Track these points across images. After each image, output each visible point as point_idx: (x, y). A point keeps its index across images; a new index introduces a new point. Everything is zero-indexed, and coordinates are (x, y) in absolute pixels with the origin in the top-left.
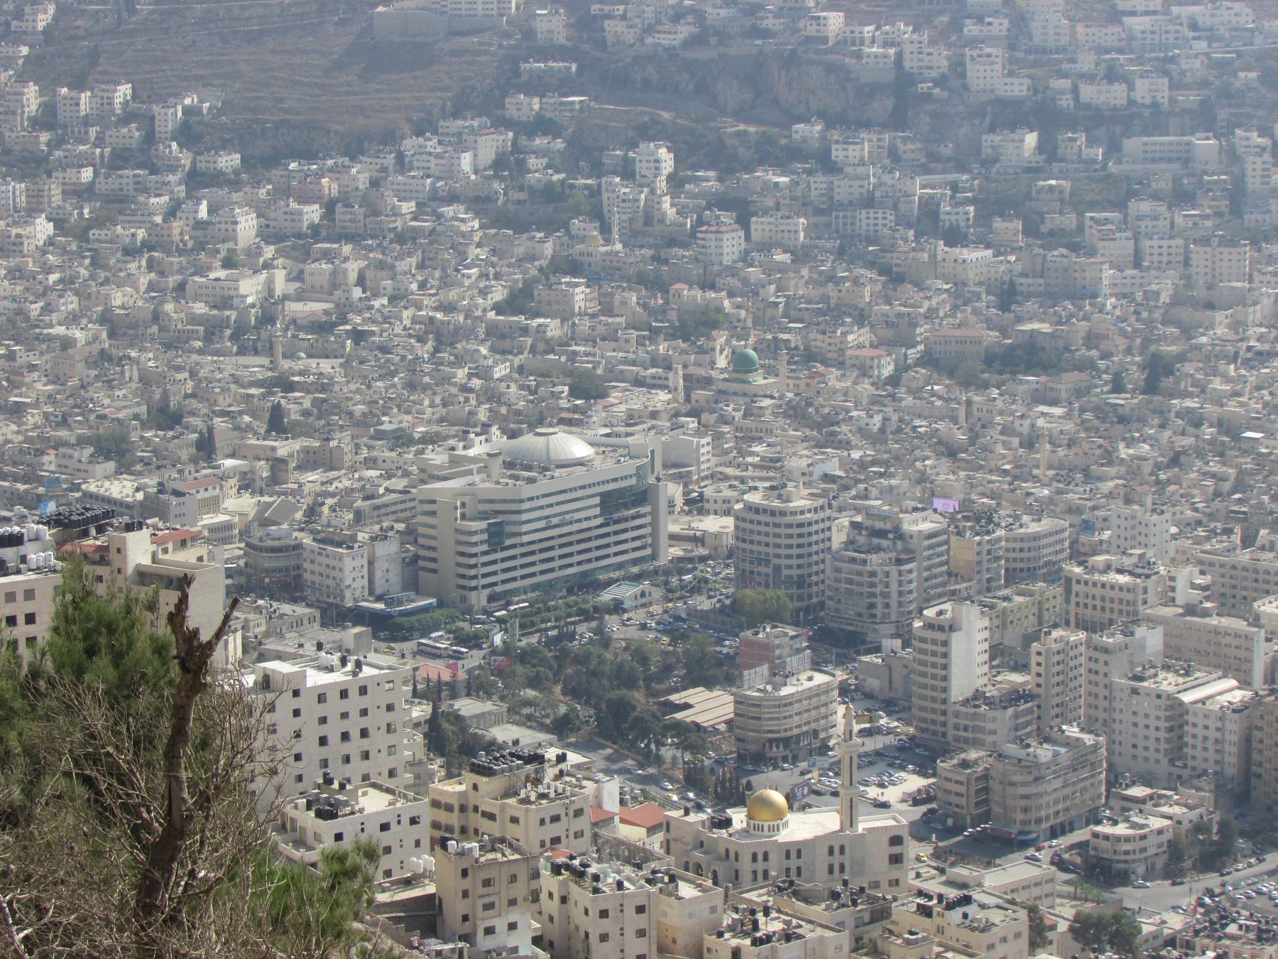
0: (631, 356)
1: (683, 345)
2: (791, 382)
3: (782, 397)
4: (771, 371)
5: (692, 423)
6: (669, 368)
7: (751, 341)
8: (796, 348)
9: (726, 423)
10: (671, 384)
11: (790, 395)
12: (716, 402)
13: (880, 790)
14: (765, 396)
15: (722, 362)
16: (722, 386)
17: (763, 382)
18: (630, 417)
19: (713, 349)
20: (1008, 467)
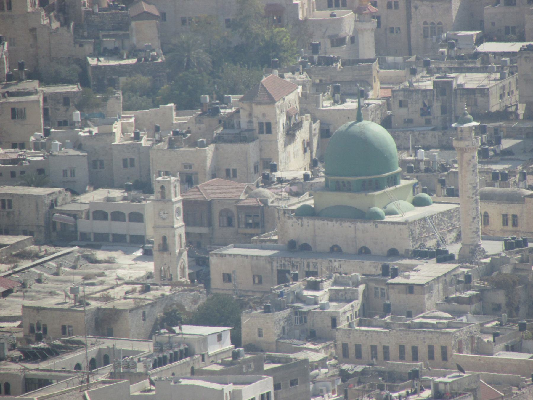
0: (36, 157)
1: (180, 120)
2: (495, 211)
3: (470, 254)
4: (435, 181)
5: (215, 341)
6: (144, 186)
7: (376, 96)
8: (504, 115)
9: (313, 336)
10: (150, 232)
11: (494, 248)
12: (283, 277)
13: (111, 195)
14: (423, 254)
15: (293, 162)
16: (298, 230)
17: (415, 213)
18: (37, 331)
19: (268, 128)
20: (276, 238)
